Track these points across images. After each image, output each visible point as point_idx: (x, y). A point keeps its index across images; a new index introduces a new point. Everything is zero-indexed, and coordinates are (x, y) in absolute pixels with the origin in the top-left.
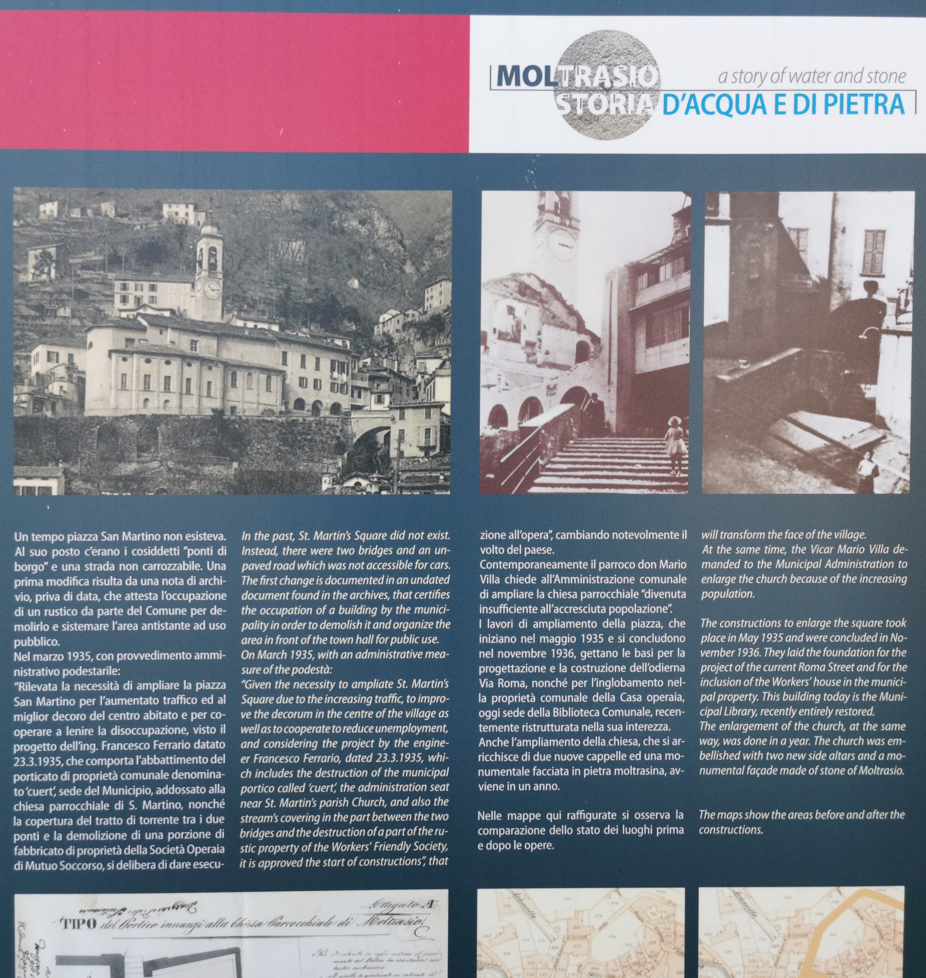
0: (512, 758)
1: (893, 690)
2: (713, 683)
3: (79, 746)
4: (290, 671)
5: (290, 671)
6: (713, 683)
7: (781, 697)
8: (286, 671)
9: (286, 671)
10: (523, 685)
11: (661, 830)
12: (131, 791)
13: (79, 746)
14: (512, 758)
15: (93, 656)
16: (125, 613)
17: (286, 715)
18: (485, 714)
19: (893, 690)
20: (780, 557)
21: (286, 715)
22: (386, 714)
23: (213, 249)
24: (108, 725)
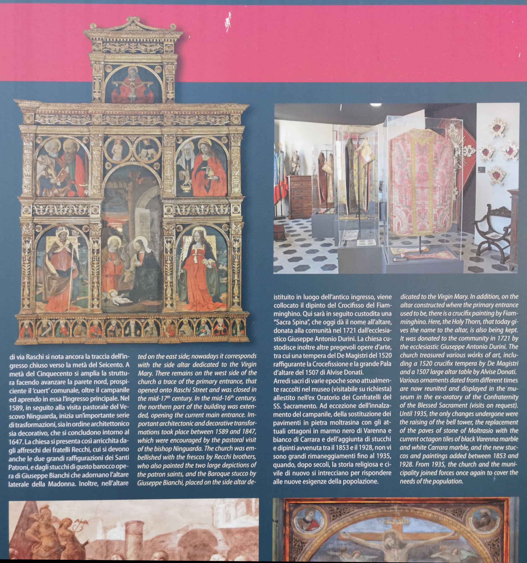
0: (292, 348)
1: (121, 479)
2: (511, 356)
3: (369, 406)
4: (472, 306)
5: (472, 306)
6: (511, 356)
7: (205, 457)
8: (469, 305)
9: (469, 305)
10: (88, 450)
11: (345, 482)
12: (103, 399)
13: (369, 406)
14: (292, 348)
15: (500, 297)
16: (284, 474)
17: (214, 424)
18: (327, 323)
19: (121, 479)
20: (470, 426)
21: (214, 424)
22: (435, 422)
23: (242, 322)
24: (423, 393)
